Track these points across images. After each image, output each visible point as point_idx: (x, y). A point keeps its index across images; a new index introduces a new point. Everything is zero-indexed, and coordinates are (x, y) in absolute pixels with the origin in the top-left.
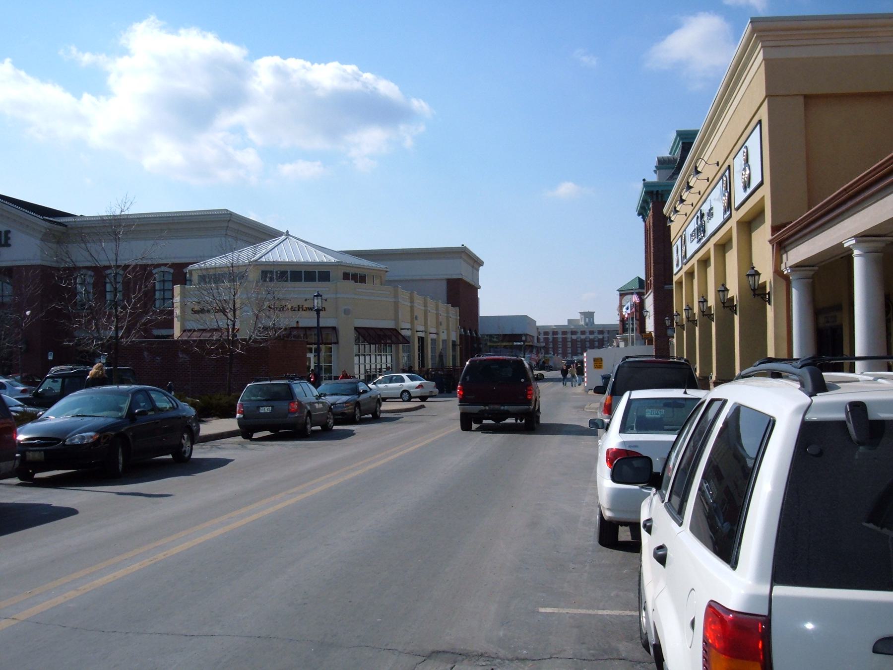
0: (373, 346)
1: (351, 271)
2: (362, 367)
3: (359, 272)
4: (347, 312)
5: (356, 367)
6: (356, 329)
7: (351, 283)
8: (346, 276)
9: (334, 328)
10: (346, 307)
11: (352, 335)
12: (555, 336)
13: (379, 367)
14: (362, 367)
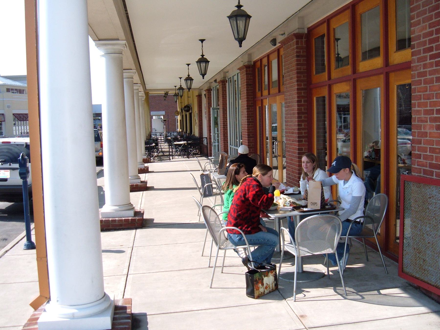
0: (22, 122)
1: (10, 88)
2: (17, 132)
3: (18, 88)
4: (9, 107)
5: (14, 132)
6: (13, 114)
7: (10, 94)
8: (8, 90)
9: (3, 114)
10: (8, 105)
11: (12, 117)
12: (411, 7)
13: (25, 131)
14: (17, 132)
